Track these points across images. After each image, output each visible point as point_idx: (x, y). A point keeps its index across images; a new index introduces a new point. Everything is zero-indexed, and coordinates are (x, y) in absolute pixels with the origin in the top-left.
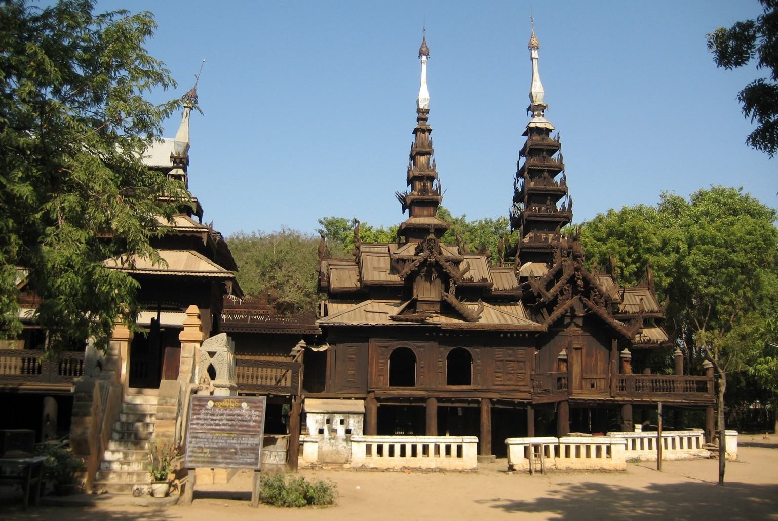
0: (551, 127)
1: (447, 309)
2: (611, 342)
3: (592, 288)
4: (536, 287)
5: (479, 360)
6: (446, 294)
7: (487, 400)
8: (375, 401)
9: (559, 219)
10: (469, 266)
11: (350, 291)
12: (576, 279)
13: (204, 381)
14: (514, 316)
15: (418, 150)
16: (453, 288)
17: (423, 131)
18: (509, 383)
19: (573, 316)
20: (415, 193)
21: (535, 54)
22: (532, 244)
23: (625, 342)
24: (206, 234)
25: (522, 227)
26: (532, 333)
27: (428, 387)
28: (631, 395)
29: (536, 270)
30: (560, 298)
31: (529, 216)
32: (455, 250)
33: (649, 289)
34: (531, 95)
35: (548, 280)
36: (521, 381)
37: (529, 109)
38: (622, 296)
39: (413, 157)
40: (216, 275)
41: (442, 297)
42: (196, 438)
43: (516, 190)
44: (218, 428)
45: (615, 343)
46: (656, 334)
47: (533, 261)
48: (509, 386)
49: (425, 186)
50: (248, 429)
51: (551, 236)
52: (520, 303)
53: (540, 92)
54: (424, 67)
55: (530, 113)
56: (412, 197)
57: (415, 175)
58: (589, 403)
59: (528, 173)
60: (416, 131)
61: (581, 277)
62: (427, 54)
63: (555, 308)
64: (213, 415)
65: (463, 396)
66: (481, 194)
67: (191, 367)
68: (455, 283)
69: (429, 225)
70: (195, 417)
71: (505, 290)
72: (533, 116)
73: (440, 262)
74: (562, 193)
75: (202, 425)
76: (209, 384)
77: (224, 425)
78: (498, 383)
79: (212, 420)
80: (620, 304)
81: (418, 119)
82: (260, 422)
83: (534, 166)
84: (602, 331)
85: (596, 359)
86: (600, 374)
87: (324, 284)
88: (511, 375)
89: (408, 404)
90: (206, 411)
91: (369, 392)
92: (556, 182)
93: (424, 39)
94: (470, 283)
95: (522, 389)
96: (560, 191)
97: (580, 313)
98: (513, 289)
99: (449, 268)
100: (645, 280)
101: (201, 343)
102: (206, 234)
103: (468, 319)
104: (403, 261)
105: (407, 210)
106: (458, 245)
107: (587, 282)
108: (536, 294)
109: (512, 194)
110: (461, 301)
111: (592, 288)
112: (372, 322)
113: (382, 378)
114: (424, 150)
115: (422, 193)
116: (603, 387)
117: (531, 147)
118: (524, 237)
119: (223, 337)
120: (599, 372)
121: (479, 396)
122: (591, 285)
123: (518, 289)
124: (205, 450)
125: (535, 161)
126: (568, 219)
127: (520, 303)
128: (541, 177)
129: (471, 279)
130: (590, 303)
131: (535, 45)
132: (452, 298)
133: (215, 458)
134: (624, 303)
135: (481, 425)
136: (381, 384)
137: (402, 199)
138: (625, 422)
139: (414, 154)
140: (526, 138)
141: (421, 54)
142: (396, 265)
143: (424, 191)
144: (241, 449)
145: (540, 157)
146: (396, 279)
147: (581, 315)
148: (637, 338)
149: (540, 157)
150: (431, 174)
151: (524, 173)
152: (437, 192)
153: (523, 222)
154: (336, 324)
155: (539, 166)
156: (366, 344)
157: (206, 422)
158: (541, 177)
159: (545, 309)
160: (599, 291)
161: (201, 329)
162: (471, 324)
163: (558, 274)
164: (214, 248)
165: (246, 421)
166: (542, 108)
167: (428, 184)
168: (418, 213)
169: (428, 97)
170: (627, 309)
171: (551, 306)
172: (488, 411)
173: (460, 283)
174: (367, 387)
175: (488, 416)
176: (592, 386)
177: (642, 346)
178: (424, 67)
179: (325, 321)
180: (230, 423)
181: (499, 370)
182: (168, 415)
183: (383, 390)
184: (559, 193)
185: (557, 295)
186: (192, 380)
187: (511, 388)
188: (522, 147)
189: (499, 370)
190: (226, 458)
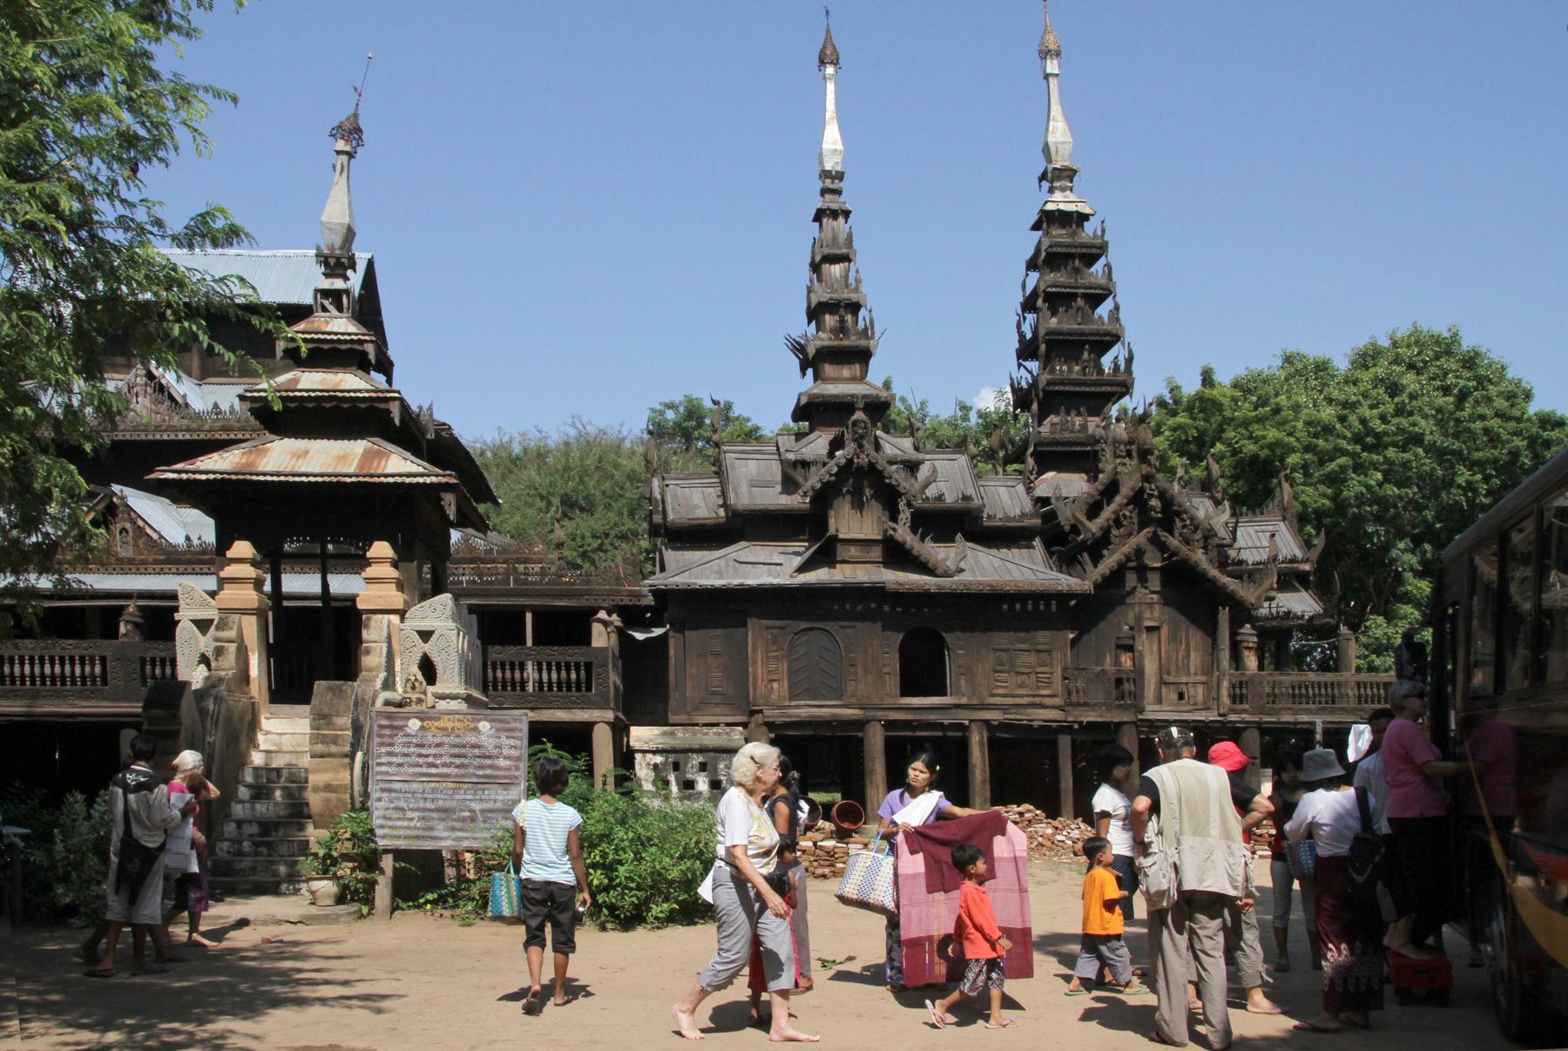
0: (1087, 210)
1: (896, 555)
2: (1215, 615)
3: (1178, 514)
4: (1065, 517)
6: (891, 524)
8: (764, 729)
10: (934, 470)
13: (413, 688)
14: (1024, 569)
15: (826, 251)
16: (905, 515)
17: (834, 214)
18: (1022, 691)
19: (1143, 571)
20: (822, 335)
21: (1052, 66)
22: (1057, 436)
23: (1242, 613)
24: (397, 403)
25: (1035, 406)
26: (1062, 597)
27: (865, 701)
28: (1261, 711)
29: (1070, 486)
30: (1115, 532)
31: (1049, 383)
32: (907, 443)
33: (1284, 519)
34: (1046, 150)
35: (1091, 501)
37: (1043, 177)
38: (1234, 532)
39: (815, 267)
40: (421, 480)
41: (885, 531)
42: (390, 791)
43: (1022, 336)
44: (433, 771)
45: (1224, 615)
46: (1302, 604)
47: (1060, 470)
49: (842, 321)
50: (496, 773)
51: (1093, 423)
52: (1037, 542)
54: (830, 87)
55: (1046, 185)
56: (819, 343)
60: (819, 216)
62: (835, 63)
63: (1105, 552)
64: (422, 746)
65: (932, 717)
66: (953, 361)
67: (383, 659)
68: (909, 505)
69: (852, 396)
70: (383, 750)
71: (1007, 518)
72: (1051, 191)
75: (400, 765)
76: (425, 693)
77: (445, 765)
78: (1000, 691)
79: (420, 755)
80: (1230, 546)
81: (824, 192)
82: (519, 759)
84: (1197, 596)
85: (1188, 650)
87: (657, 519)
89: (939, 734)
90: (406, 739)
91: (752, 713)
92: (1100, 317)
93: (828, 31)
94: (939, 505)
95: (1047, 701)
96: (1108, 334)
97: (1154, 561)
98: (1023, 515)
99: (897, 475)
100: (1276, 501)
101: (402, 614)
102: (397, 403)
104: (805, 464)
105: (810, 371)
106: (912, 434)
107: (1164, 497)
108: (1067, 528)
109: (1015, 344)
110: (922, 539)
111: (1178, 514)
112: (752, 582)
113: (775, 685)
114: (838, 252)
115: (837, 336)
116: (1200, 697)
118: (1040, 425)
119: (446, 598)
121: (964, 717)
123: (1032, 516)
124: (410, 814)
125: (1059, 278)
127: (1037, 542)
129: (940, 498)
130: (1174, 542)
131: (1052, 47)
132: (903, 533)
133: (431, 828)
134: (1237, 545)
136: (774, 697)
137: (799, 349)
139: (818, 258)
140: (1040, 233)
141: (822, 63)
143: (841, 329)
144: (483, 811)
145: (1066, 268)
146: (796, 501)
148: (1264, 611)
149: (1066, 268)
150: (854, 297)
152: (866, 333)
156: (741, 630)
157: (408, 759)
159: (1085, 555)
160: (1192, 519)
161: (401, 587)
163: (1111, 490)
164: (439, 447)
165: (490, 757)
167: (849, 318)
169: (839, 146)
170: (1245, 555)
171: (1097, 548)
173: (918, 503)
176: (1181, 696)
178: (830, 87)
179: (659, 580)
180: (458, 761)
182: (333, 749)
186: (389, 684)
188: (1030, 252)
190: (453, 829)
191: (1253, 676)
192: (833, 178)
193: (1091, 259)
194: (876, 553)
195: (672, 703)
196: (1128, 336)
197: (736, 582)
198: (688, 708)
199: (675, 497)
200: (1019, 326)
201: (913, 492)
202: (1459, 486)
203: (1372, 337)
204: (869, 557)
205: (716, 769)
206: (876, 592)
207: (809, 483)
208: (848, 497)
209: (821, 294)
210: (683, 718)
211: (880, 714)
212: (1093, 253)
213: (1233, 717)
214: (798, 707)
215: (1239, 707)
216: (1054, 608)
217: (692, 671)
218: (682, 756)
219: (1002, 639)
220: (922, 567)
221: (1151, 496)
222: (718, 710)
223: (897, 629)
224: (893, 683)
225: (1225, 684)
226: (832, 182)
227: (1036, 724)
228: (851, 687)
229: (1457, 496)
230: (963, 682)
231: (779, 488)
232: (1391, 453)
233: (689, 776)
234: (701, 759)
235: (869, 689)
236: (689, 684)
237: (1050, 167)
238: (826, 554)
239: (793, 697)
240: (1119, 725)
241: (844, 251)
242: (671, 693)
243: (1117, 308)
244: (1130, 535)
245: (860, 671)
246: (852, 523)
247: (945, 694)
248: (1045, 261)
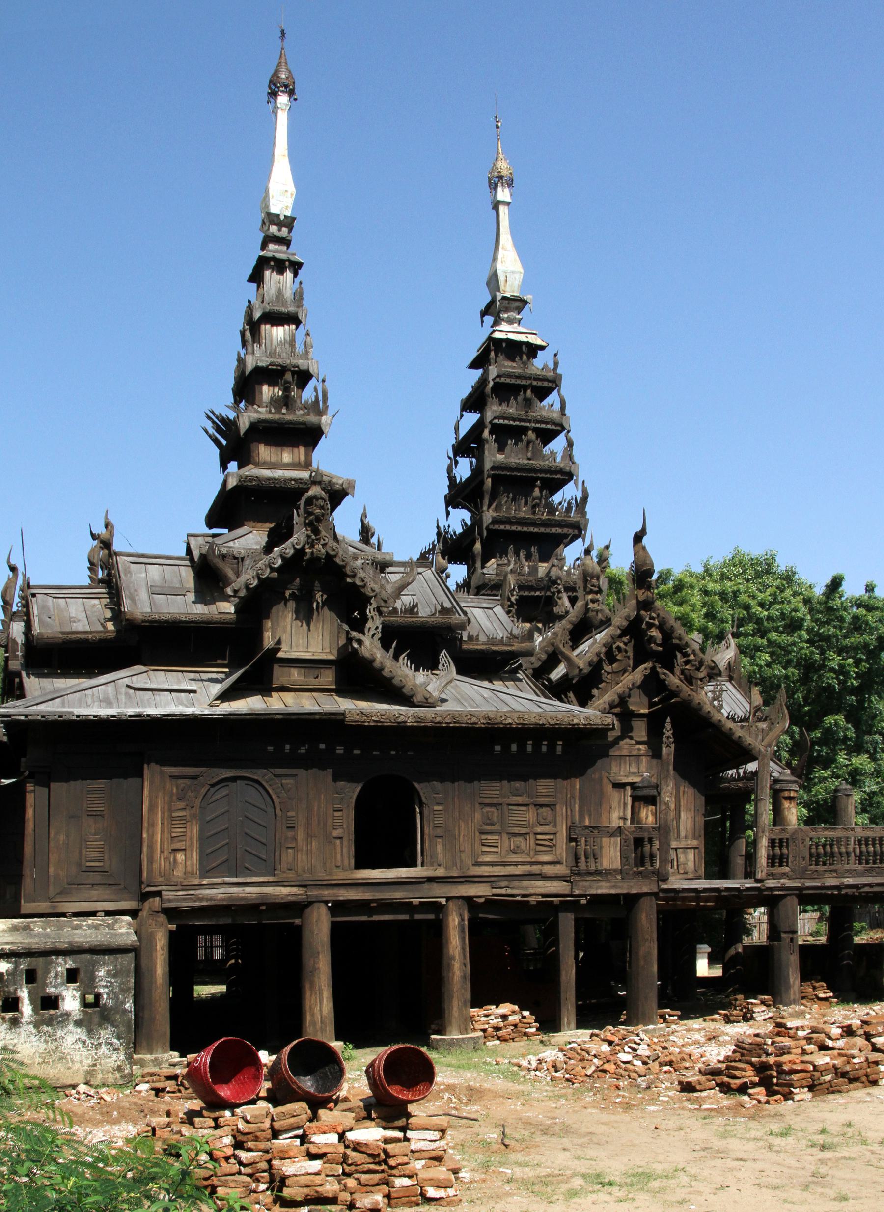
0: (539, 342)
1: (355, 675)
5: (438, 804)
7: (460, 902)
8: (162, 918)
9: (565, 530)
11: (87, 640)
12: (644, 626)
16: (374, 624)
27: (307, 876)
28: (802, 875)
30: (607, 668)
31: (495, 521)
34: (494, 276)
36: (545, 853)
48: (516, 864)
53: (513, 272)
54: (283, 118)
55: (489, 320)
57: (260, 364)
58: (684, 899)
59: (491, 433)
61: (656, 622)
63: (595, 692)
65: (398, 895)
68: (378, 610)
71: (492, 641)
72: (496, 323)
73: (338, 560)
74: (560, 478)
78: (488, 858)
81: (268, 239)
83: (504, 418)
86: (686, 837)
88: (521, 839)
89: (405, 917)
91: (145, 897)
94: (409, 619)
95: (548, 870)
96: (560, 471)
103: (415, 699)
113: (180, 857)
114: (283, 310)
115: (269, 415)
116: (691, 865)
117: (498, 380)
120: (683, 834)
121: (439, 893)
122: (675, 641)
126: (577, 530)
128: (521, 441)
129: (412, 610)
130: (674, 680)
132: (370, 646)
135: (445, 962)
136: (179, 873)
138: (783, 935)
139: (257, 315)
142: (208, 575)
143: (286, 401)
145: (510, 415)
147: (642, 711)
149: (510, 415)
150: (302, 364)
151: (483, 431)
152: (318, 407)
153: (480, 534)
154: (50, 718)
155: (514, 420)
156: (133, 781)
158: (521, 441)
162: (425, 713)
166: (517, 304)
168: (268, 459)
172: (462, 930)
174: (141, 883)
175: (463, 939)
177: (740, 784)
178: (283, 118)
181: (488, 828)
183: (185, 887)
184: (559, 476)
185: (600, 661)
187: (519, 870)
189: (488, 828)
191: (795, 832)
192: (280, 225)
193: (543, 393)
194: (328, 678)
195: (28, 884)
196: (582, 474)
197: (131, 711)
198: (52, 891)
199: (43, 608)
200: (449, 470)
201: (384, 595)
202: (832, 670)
203: (688, 565)
204: (314, 683)
205: (92, 978)
206: (331, 727)
207: (242, 579)
208: (292, 604)
209: (256, 359)
210: (43, 906)
211: (327, 893)
212: (545, 386)
213: (771, 883)
214: (212, 886)
215: (778, 870)
216: (559, 749)
217: (59, 836)
218: (41, 960)
219: (494, 790)
220: (393, 692)
221: (650, 626)
222: (94, 893)
223: (351, 779)
224: (345, 851)
225: (764, 842)
226: (278, 229)
227: (533, 900)
228: (288, 856)
229: (829, 678)
230: (439, 848)
231: (191, 597)
232: (774, 636)
233: (51, 990)
234: (70, 964)
235: (311, 858)
236: (54, 858)
237: (499, 296)
238: (258, 675)
239: (205, 872)
240: (638, 896)
241: (292, 309)
242: (27, 871)
243: (570, 444)
244: (624, 671)
245: (301, 835)
246: (300, 637)
247: (411, 862)
248: (493, 389)
